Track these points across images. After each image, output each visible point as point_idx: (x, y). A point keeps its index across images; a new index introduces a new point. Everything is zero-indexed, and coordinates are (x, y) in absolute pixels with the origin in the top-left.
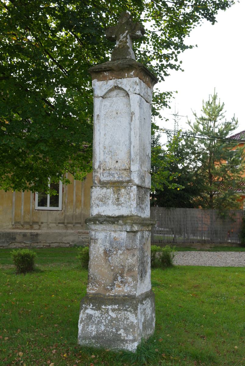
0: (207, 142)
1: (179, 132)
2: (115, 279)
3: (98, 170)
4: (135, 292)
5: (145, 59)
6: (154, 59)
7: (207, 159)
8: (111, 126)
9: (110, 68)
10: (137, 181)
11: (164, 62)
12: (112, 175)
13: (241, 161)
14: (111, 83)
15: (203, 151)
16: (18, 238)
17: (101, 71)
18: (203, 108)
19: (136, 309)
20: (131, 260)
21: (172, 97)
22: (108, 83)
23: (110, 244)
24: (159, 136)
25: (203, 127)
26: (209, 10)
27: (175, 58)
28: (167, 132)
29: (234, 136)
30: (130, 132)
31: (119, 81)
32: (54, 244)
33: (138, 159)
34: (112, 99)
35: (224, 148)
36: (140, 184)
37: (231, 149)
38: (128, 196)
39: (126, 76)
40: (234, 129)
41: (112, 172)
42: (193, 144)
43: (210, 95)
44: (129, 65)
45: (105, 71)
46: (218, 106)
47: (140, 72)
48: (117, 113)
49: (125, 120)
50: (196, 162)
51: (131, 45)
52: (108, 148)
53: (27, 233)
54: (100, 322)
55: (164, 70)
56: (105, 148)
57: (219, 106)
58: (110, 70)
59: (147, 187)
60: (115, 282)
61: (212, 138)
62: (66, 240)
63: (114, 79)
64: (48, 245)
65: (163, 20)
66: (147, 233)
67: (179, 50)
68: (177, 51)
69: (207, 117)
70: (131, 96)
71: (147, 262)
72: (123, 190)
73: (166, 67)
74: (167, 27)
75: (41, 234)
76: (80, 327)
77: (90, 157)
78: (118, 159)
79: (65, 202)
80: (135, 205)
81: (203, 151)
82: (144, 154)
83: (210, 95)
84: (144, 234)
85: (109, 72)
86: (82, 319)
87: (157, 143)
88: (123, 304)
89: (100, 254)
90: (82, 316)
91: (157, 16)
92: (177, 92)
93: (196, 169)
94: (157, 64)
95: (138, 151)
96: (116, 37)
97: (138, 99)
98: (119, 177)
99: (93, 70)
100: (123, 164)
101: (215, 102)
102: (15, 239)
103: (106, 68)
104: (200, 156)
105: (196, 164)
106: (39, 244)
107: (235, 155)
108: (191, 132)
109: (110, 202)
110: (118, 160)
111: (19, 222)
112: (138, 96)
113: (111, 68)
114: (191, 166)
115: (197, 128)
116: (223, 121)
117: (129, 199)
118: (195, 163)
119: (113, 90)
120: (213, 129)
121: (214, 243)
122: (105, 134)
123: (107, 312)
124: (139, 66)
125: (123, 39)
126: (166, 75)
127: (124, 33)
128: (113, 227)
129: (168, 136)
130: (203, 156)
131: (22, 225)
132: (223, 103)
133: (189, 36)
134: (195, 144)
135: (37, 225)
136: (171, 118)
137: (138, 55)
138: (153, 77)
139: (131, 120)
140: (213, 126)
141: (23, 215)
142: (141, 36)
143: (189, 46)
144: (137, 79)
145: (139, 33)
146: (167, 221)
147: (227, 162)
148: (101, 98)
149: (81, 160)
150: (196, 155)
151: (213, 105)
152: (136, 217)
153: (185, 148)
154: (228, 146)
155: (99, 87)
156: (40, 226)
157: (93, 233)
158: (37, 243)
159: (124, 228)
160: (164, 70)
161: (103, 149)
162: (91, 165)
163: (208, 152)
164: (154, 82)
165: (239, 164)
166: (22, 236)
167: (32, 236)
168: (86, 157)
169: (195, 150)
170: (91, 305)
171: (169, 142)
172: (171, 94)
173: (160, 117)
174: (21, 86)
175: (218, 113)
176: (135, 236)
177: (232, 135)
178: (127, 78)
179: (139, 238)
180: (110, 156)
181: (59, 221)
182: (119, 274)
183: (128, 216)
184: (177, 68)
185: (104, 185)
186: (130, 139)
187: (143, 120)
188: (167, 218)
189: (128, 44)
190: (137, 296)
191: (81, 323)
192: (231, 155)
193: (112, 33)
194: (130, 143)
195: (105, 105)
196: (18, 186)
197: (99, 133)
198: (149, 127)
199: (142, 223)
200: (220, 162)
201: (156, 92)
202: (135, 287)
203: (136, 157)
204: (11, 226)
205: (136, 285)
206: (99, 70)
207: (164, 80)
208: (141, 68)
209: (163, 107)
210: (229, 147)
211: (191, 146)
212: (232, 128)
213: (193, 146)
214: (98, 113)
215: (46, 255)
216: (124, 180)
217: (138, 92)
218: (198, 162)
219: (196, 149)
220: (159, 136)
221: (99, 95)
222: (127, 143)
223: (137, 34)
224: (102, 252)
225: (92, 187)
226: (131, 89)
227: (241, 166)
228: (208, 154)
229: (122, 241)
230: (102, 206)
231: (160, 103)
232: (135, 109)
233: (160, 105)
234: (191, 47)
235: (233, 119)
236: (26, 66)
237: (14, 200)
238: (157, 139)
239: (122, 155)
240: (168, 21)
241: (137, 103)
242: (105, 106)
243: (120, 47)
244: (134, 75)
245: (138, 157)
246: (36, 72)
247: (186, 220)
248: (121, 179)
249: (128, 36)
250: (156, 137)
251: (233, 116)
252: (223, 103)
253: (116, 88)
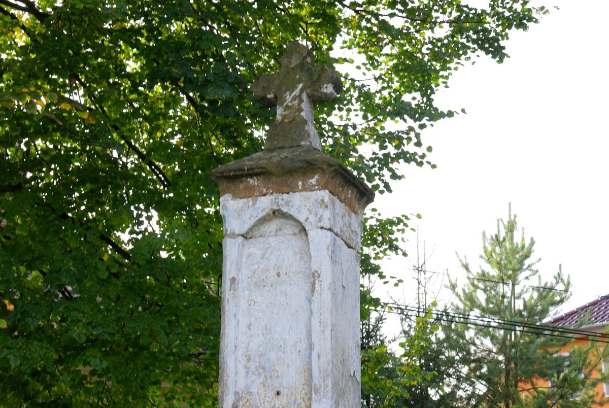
0: (497, 335)
1: (427, 312)
5: (346, 142)
6: (366, 141)
7: (499, 376)
8: (264, 305)
9: (261, 168)
11: (391, 150)
13: (583, 382)
14: (265, 203)
15: (488, 355)
17: (242, 176)
18: (485, 252)
21: (410, 228)
22: (258, 202)
24: (380, 319)
25: (485, 297)
26: (490, 32)
27: (415, 140)
28: (403, 311)
29: (561, 319)
30: (310, 319)
31: (283, 200)
33: (330, 386)
34: (267, 242)
35: (540, 348)
37: (557, 352)
39: (300, 187)
40: (562, 301)
42: (464, 338)
43: (500, 221)
44: (307, 162)
45: (251, 176)
46: (520, 245)
47: (333, 178)
48: (278, 275)
49: (297, 291)
50: (472, 384)
51: (310, 116)
52: (257, 359)
55: (391, 165)
56: (249, 360)
57: (523, 247)
58: (262, 173)
61: (509, 326)
63: (272, 193)
65: (384, 55)
67: (424, 121)
68: (418, 123)
69: (493, 272)
70: (313, 233)
73: (393, 160)
74: (395, 69)
77: (214, 373)
78: (281, 385)
81: (488, 355)
82: (343, 374)
83: (500, 221)
84: (472, 321)
85: (259, 178)
87: (376, 336)
91: (370, 43)
92: (419, 216)
93: (473, 402)
94: (374, 153)
95: (330, 368)
96: (276, 97)
99: (222, 173)
100: (293, 398)
101: (512, 238)
103: (252, 169)
104: (482, 368)
105: (474, 388)
107: (569, 366)
108: (458, 308)
110: (281, 389)
112: (329, 233)
113: (265, 168)
114: (460, 393)
115: (471, 301)
116: (534, 282)
118: (471, 385)
119: (270, 220)
120: (510, 303)
122: (250, 324)
124: (330, 165)
125: (291, 101)
126: (394, 176)
127: (293, 88)
129: (402, 320)
130: (488, 368)
132: (532, 239)
133: (447, 87)
134: (467, 337)
136: (409, 277)
137: (327, 132)
138: (362, 188)
139: (313, 290)
140: (509, 294)
142: (333, 96)
143: (446, 113)
144: (325, 194)
145: (328, 89)
147: (549, 384)
148: (240, 239)
149: (192, 382)
150: (473, 365)
151: (508, 245)
153: (444, 347)
154: (550, 343)
155: (236, 211)
160: (391, 165)
161: (244, 360)
162: (215, 394)
163: (501, 358)
164: (366, 199)
165: (580, 390)
168: (205, 376)
169: (469, 353)
171: (405, 332)
172: (406, 221)
173: (382, 276)
174: (53, 211)
175: (521, 263)
177: (558, 316)
178: (300, 191)
180: (262, 379)
184: (419, 160)
186: (309, 336)
187: (339, 289)
189: (303, 114)
192: (558, 365)
193: (266, 89)
194: (311, 347)
195: (249, 255)
197: (234, 321)
198: (355, 306)
200: (533, 384)
201: (372, 217)
203: (324, 380)
206: (238, 173)
207: (390, 191)
208: (333, 168)
209: (388, 252)
210: (552, 346)
211: (458, 342)
212: (558, 298)
213: (464, 344)
214: (233, 274)
217: (327, 225)
218: (477, 382)
219: (472, 351)
220: (381, 319)
221: (237, 232)
222: (303, 346)
223: (325, 91)
226: (312, 219)
227: (586, 393)
228: (500, 362)
231: (382, 243)
232: (321, 265)
233: (382, 249)
234: (450, 114)
235: (559, 278)
236: (64, 160)
238: (377, 328)
240: (397, 57)
241: (326, 251)
242: (251, 258)
243: (286, 120)
244: (318, 184)
245: (329, 382)
246: (88, 175)
249: (304, 97)
250: (373, 321)
251: (558, 270)
252: (532, 239)
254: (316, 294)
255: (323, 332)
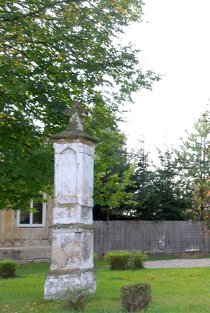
2: (68, 260)
3: (58, 197)
4: (79, 267)
10: (81, 203)
12: (67, 200)
14: (66, 145)
19: (80, 276)
20: (78, 249)
23: (65, 240)
32: (37, 260)
36: (83, 205)
38: (75, 212)
41: (66, 198)
45: (62, 138)
48: (69, 163)
49: (74, 168)
53: (8, 250)
54: (58, 285)
56: (62, 184)
59: (89, 206)
60: (67, 262)
62: (49, 256)
64: (31, 261)
70: (78, 154)
71: (89, 251)
72: (72, 209)
75: (23, 251)
76: (45, 290)
78: (70, 190)
79: (49, 219)
80: (80, 217)
86: (47, 285)
88: (72, 273)
89: (59, 247)
90: (47, 283)
97: (82, 155)
98: (70, 201)
106: (21, 260)
109: (65, 216)
117: (76, 213)
121: (203, 252)
123: (62, 279)
124: (82, 137)
128: (66, 230)
131: (2, 243)
135: (18, 243)
141: (3, 232)
144: (81, 144)
146: (155, 234)
152: (80, 224)
157: (54, 234)
159: (73, 230)
161: (60, 184)
166: (3, 254)
167: (14, 254)
170: (52, 276)
176: (80, 235)
179: (82, 236)
180: (65, 189)
181: (42, 238)
182: (70, 257)
183: (75, 223)
185: (61, 205)
188: (156, 230)
189: (77, 121)
190: (80, 269)
191: (46, 287)
193: (68, 113)
194: (77, 181)
195: (62, 158)
198: (91, 170)
199: (86, 227)
202: (80, 264)
205: (80, 263)
215: (28, 269)
216: (74, 203)
222: (75, 181)
223: (83, 115)
224: (60, 245)
225: (53, 207)
226: (78, 150)
229: (72, 238)
230: (60, 218)
239: (72, 188)
245: (82, 190)
247: (175, 232)
248: (72, 202)
249: (77, 116)
253: (69, 148)
254: (78, 169)
255: (80, 178)
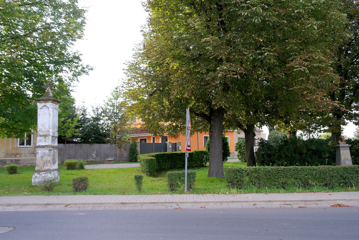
2: (44, 164)
10: (51, 134)
14: (43, 104)
16: (8, 162)
20: (50, 159)
41: (44, 132)
49: (48, 116)
64: (25, 165)
66: (56, 151)
70: (50, 109)
72: (47, 137)
76: (33, 180)
90: (33, 177)
102: (6, 163)
106: (20, 165)
111: (8, 154)
117: (49, 140)
123: (42, 174)
141: (10, 150)
144: (51, 103)
156: (20, 155)
157: (37, 151)
158: (19, 164)
159: (47, 149)
167: (16, 161)
182: (46, 163)
185: (41, 136)
196: (9, 136)
199: (54, 147)
202: (51, 166)
204: (3, 156)
237: (5, 142)
239: (47, 127)
245: (52, 128)
253: (45, 106)
